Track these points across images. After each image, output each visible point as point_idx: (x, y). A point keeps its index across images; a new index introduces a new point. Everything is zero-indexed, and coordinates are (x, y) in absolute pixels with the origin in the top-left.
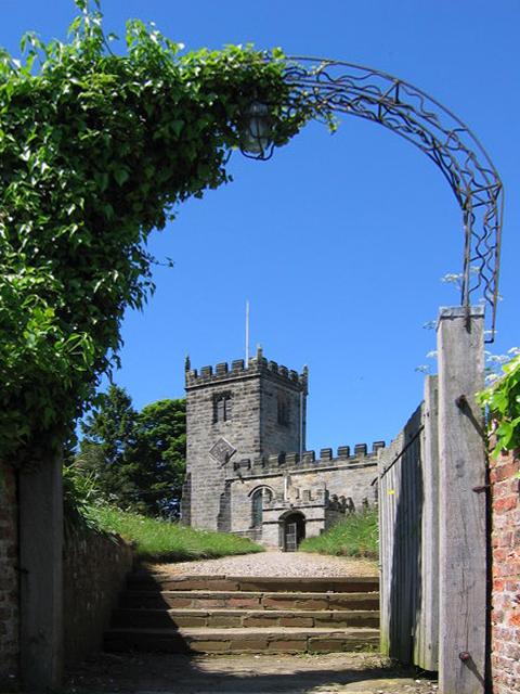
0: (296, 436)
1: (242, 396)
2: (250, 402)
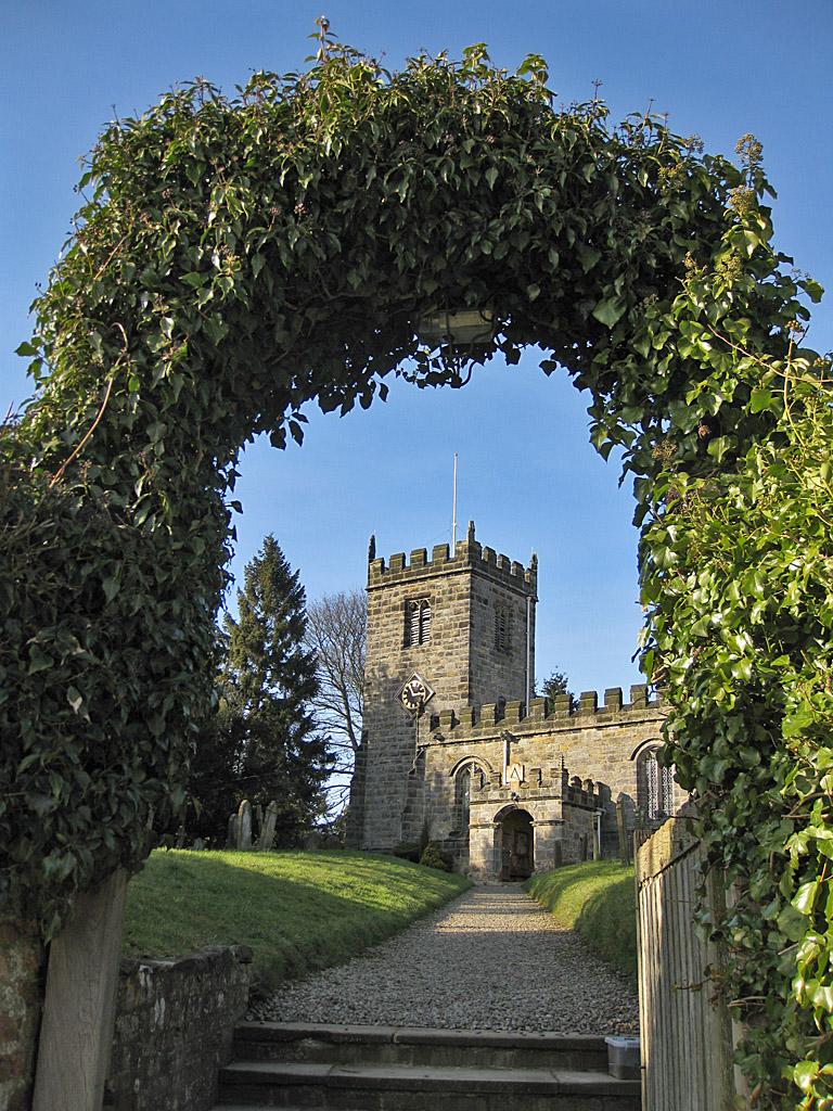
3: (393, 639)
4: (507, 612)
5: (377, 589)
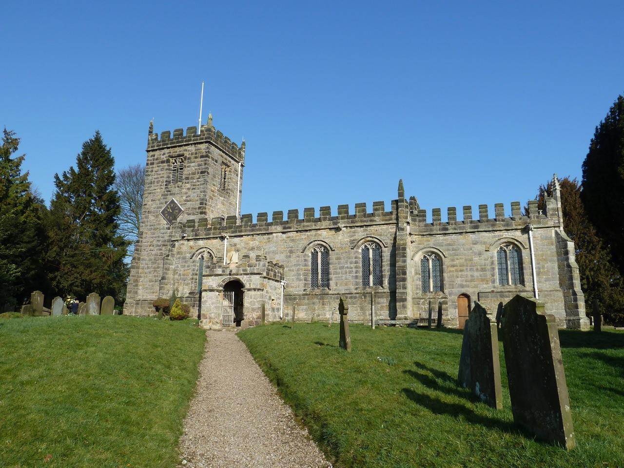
2: (199, 165)
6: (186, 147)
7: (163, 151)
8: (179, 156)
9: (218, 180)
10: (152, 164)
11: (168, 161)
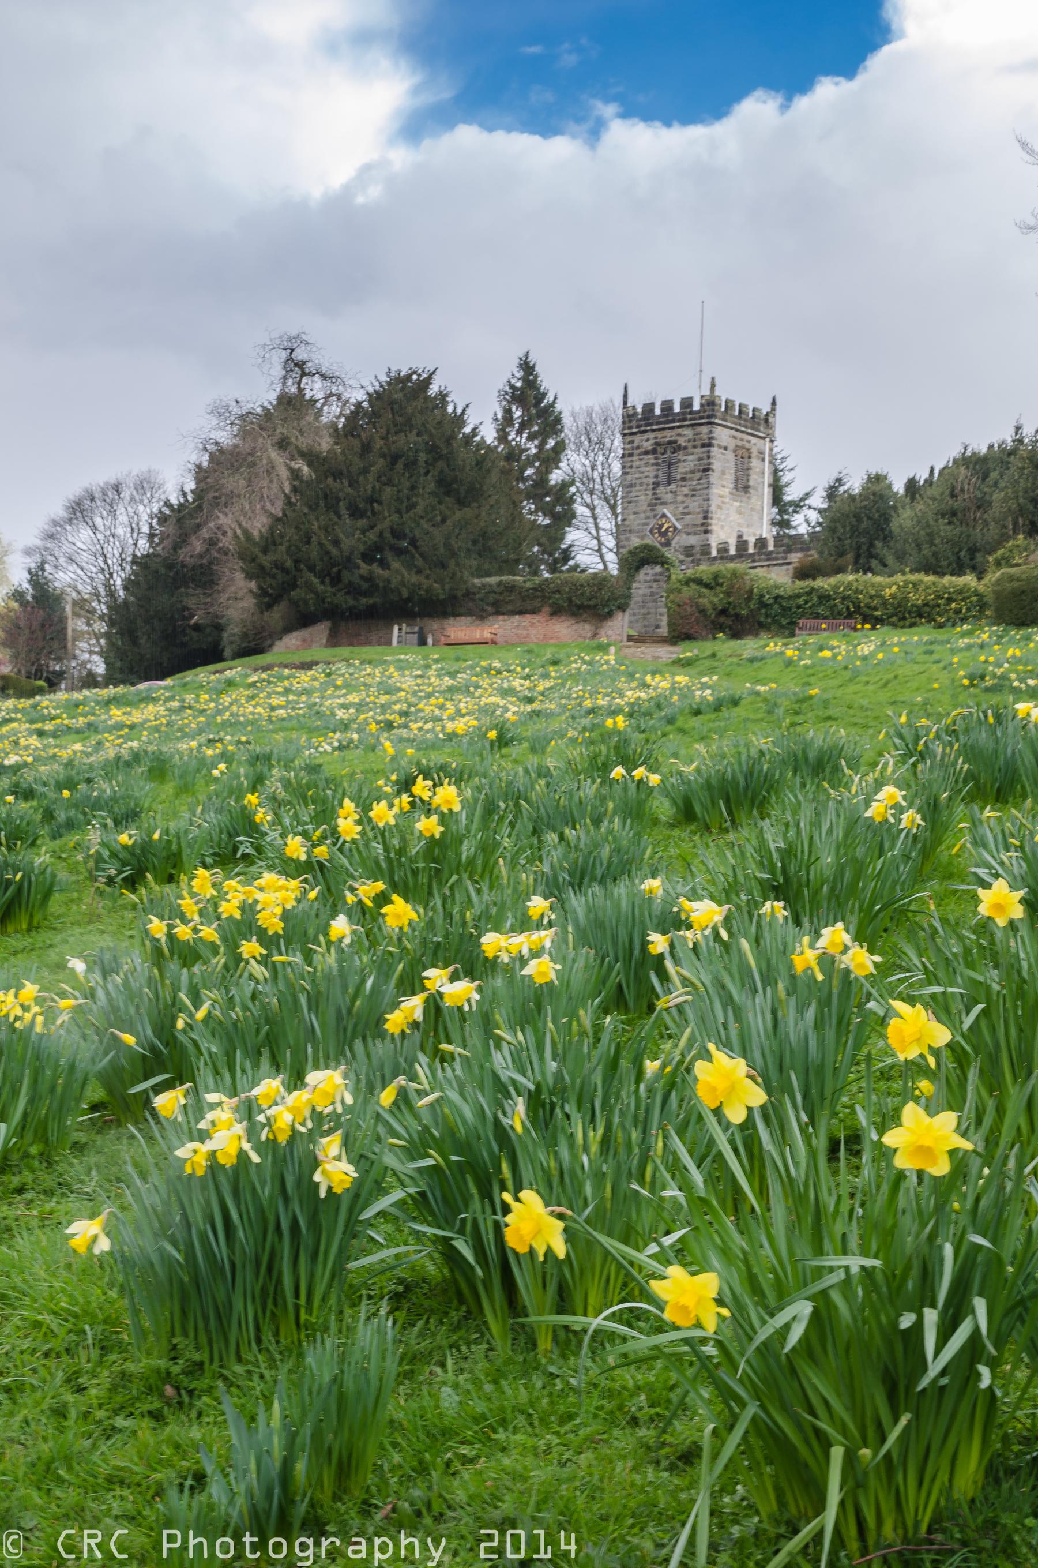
0: (758, 507)
1: (690, 450)
2: (700, 459)
3: (645, 480)
4: (746, 455)
5: (632, 434)
6: (680, 430)
7: (646, 436)
8: (670, 443)
9: (730, 477)
10: (631, 455)
11: (654, 451)
